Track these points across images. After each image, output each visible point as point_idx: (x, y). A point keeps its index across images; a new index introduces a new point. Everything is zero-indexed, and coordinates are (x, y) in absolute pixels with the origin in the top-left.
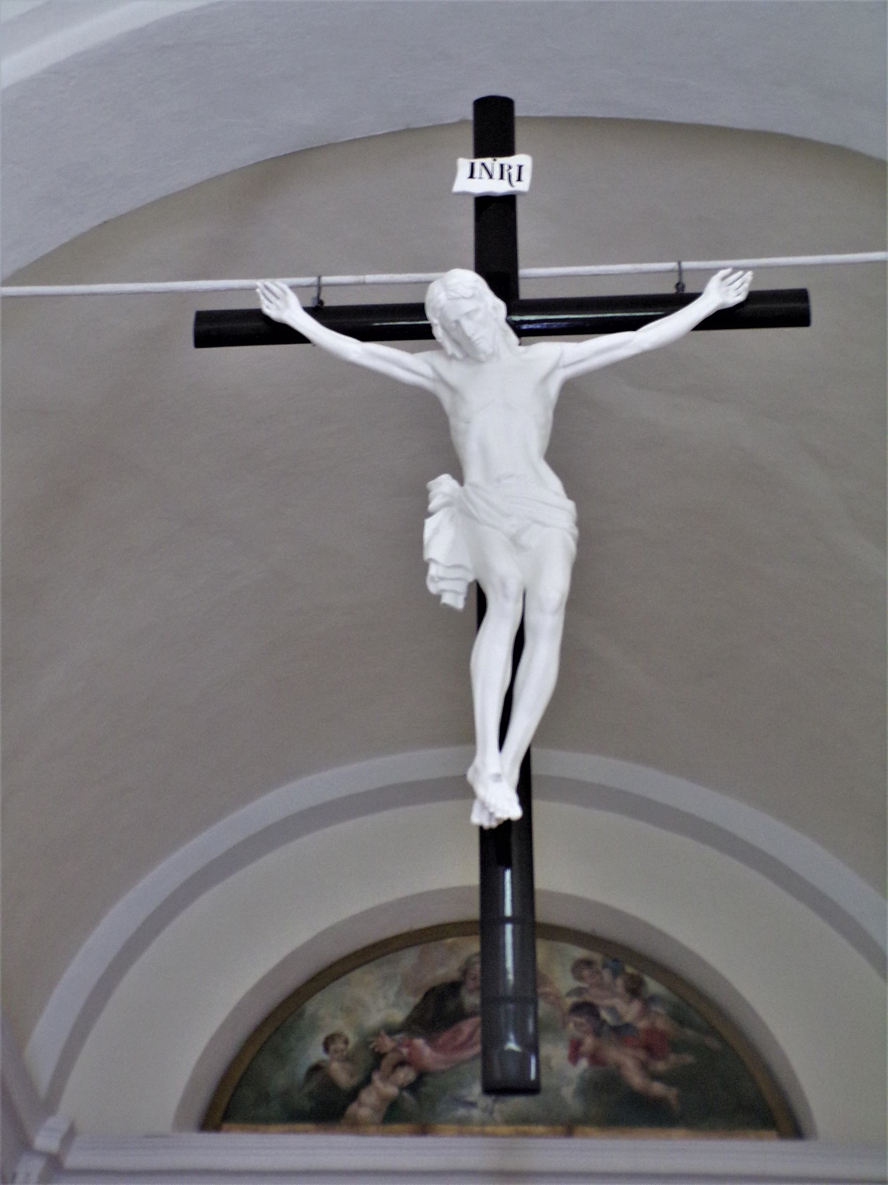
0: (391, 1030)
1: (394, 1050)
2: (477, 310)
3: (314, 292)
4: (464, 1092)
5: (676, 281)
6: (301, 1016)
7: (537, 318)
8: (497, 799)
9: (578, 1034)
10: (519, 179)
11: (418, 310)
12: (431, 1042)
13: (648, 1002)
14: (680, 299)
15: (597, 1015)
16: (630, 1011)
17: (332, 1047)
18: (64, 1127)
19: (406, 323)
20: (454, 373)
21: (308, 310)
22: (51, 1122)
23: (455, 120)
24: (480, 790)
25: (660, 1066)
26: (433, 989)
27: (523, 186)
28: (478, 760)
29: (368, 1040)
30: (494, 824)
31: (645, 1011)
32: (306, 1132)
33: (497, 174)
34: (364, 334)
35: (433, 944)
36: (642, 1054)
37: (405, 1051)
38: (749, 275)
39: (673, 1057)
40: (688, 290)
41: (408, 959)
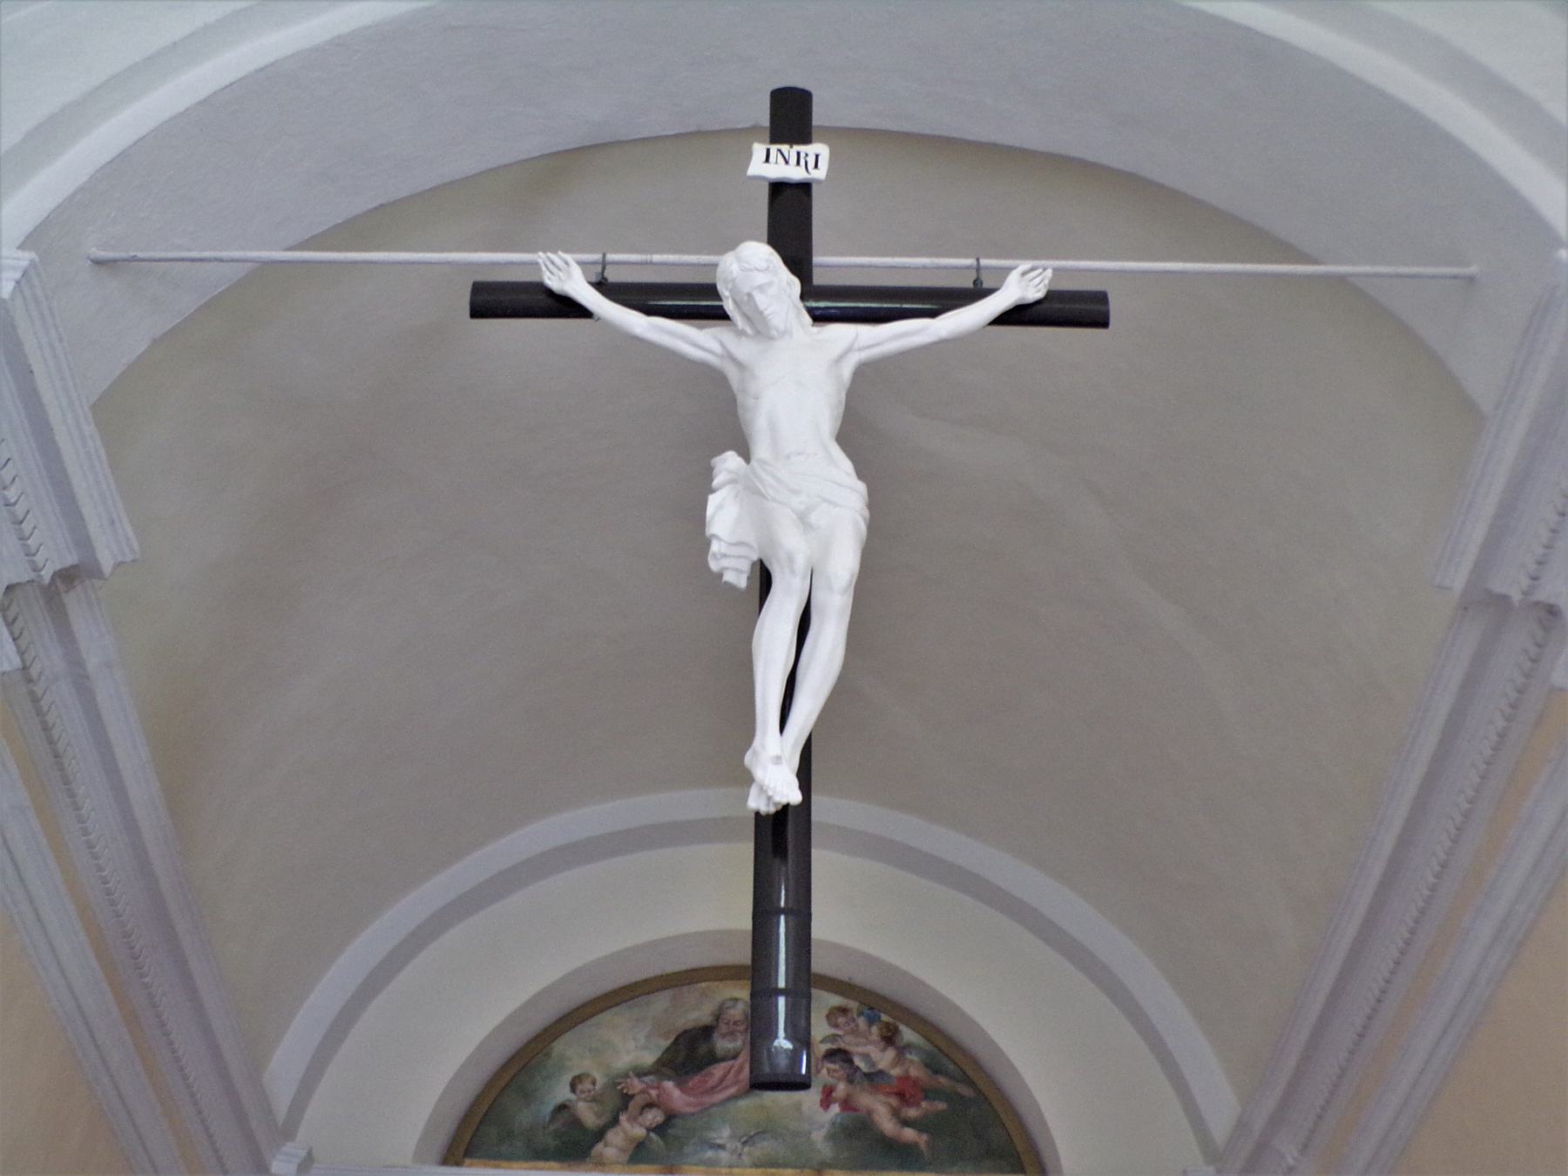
0: (640, 1073)
1: (642, 1092)
2: (770, 284)
3: (599, 269)
4: (713, 1135)
5: (974, 276)
6: (548, 1055)
7: (831, 304)
8: (775, 780)
9: (831, 1081)
10: (816, 166)
11: (711, 290)
12: (680, 1085)
13: (902, 1050)
14: (977, 293)
15: (850, 1062)
16: (884, 1059)
17: (580, 1087)
18: (303, 1153)
19: (697, 302)
20: (744, 349)
21: (592, 284)
22: (289, 1147)
23: (747, 125)
24: (759, 774)
25: (912, 1113)
26: (686, 1031)
27: (820, 174)
28: (757, 742)
29: (614, 1083)
30: (772, 810)
31: (899, 1059)
32: (549, 1169)
33: (793, 160)
34: (649, 311)
35: (685, 989)
36: (894, 1101)
37: (654, 1093)
38: (1049, 273)
39: (924, 1104)
40: (986, 285)
41: (660, 1002)
